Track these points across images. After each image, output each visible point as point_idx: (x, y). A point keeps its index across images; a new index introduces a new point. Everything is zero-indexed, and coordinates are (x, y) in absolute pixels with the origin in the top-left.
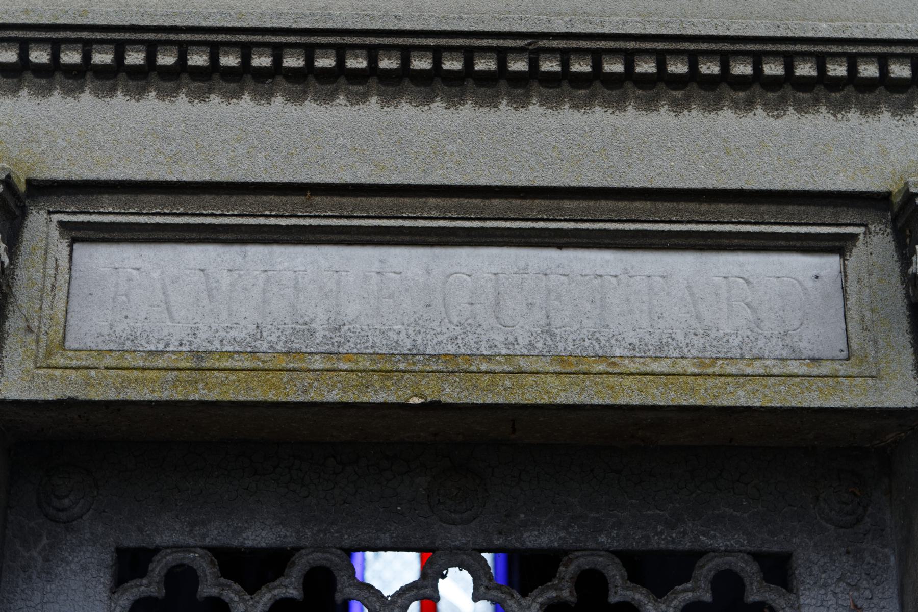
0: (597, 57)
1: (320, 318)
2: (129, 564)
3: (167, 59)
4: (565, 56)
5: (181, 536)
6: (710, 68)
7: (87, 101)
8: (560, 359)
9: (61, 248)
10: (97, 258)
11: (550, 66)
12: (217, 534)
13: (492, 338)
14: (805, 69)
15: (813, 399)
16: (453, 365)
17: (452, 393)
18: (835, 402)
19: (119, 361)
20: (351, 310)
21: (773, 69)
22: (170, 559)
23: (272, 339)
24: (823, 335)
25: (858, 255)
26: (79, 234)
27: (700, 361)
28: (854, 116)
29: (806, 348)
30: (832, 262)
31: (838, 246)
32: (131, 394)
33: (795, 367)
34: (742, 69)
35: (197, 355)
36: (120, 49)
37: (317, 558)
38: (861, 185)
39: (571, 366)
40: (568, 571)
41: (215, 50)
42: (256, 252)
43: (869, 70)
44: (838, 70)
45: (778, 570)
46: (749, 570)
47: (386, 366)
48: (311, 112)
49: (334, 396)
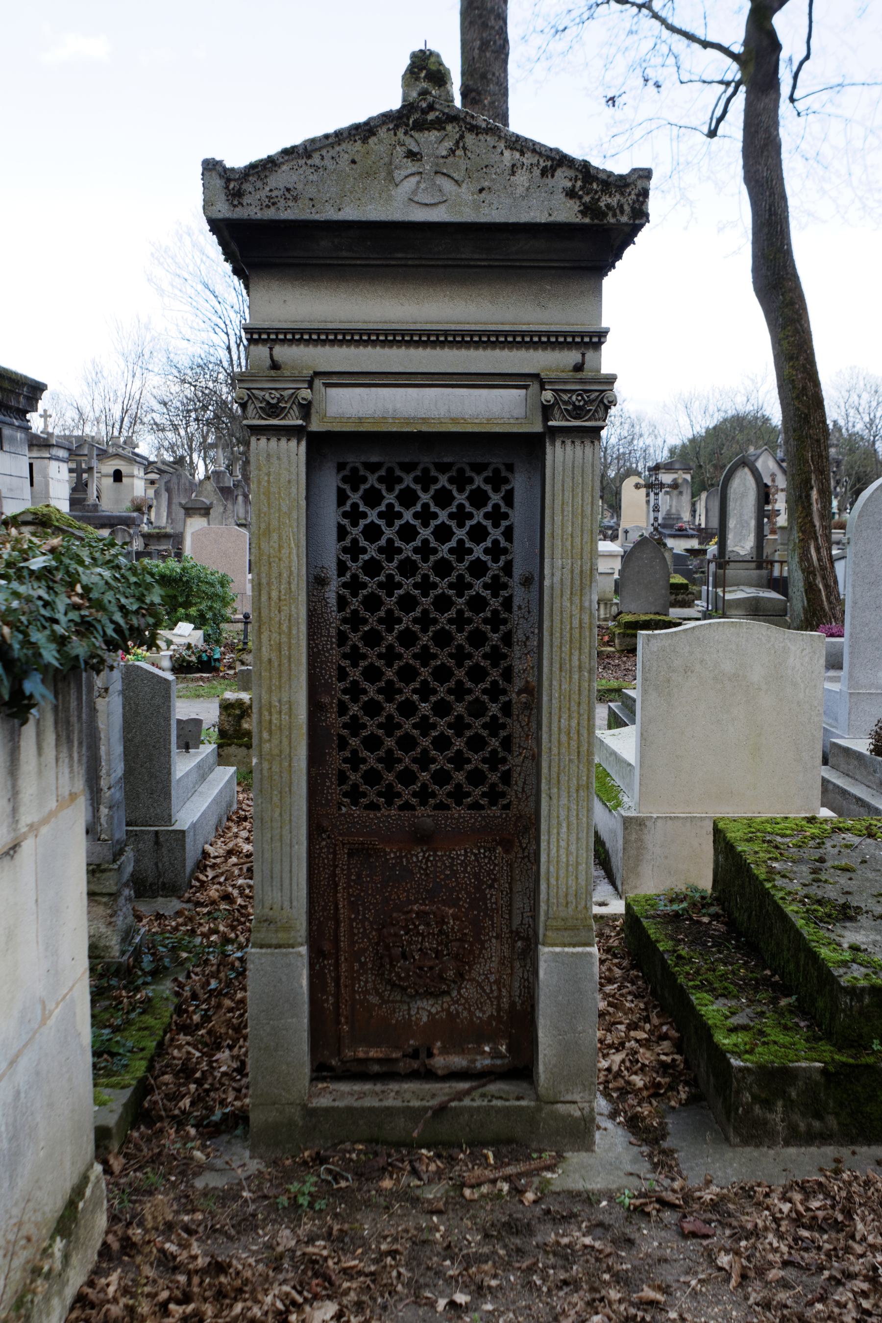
0: (463, 336)
1: (390, 407)
2: (341, 467)
3: (348, 337)
4: (454, 336)
5: (354, 459)
6: (493, 339)
7: (327, 348)
8: (452, 419)
9: (323, 389)
10: (332, 391)
11: (450, 339)
12: (363, 459)
13: (434, 414)
14: (519, 339)
15: (515, 430)
16: (425, 420)
17: (425, 428)
18: (521, 431)
19: (340, 419)
20: (398, 406)
21: (510, 339)
22: (351, 465)
23: (378, 414)
24: (519, 412)
25: (530, 389)
26: (327, 385)
27: (488, 419)
28: (531, 351)
29: (515, 415)
30: (524, 391)
31: (526, 387)
32: (344, 429)
33: (512, 421)
34: (502, 339)
35: (360, 418)
36: (336, 335)
37: (390, 465)
38: (532, 371)
39: (454, 421)
40: (455, 468)
41: (361, 335)
42: (373, 389)
43: (536, 339)
44: (527, 339)
45: (510, 468)
46: (502, 468)
47: (407, 421)
48: (387, 351)
49: (395, 429)
